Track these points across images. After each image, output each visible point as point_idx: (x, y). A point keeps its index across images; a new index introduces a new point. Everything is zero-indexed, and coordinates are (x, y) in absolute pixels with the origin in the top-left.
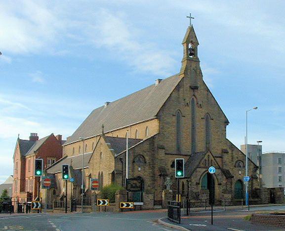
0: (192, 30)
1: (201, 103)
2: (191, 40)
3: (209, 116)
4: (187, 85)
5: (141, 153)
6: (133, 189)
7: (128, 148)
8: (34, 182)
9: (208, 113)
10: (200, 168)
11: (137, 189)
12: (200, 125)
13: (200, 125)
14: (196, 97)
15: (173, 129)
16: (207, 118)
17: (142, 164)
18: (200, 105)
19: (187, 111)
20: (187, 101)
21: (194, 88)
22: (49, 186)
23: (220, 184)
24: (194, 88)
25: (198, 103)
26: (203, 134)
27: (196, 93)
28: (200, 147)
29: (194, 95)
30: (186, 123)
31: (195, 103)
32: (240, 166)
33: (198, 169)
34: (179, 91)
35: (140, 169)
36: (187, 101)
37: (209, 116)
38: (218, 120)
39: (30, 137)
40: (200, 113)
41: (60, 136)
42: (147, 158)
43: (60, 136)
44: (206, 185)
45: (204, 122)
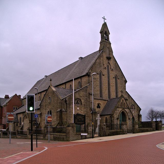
0: (105, 25)
1: (113, 68)
2: (105, 32)
3: (116, 76)
4: (105, 56)
5: (79, 98)
6: (79, 123)
7: (74, 91)
8: (161, 148)
9: (116, 75)
10: (118, 108)
11: (82, 123)
12: (113, 82)
13: (113, 82)
14: (110, 65)
15: (98, 82)
16: (116, 78)
17: (79, 105)
18: (112, 69)
19: (105, 72)
20: (105, 66)
21: (109, 58)
22: (12, 120)
23: (129, 119)
24: (109, 58)
25: (111, 68)
26: (114, 87)
27: (110, 62)
28: (113, 95)
29: (109, 63)
30: (105, 79)
31: (109, 68)
32: (133, 109)
33: (118, 109)
34: (100, 59)
35: (78, 108)
36: (105, 66)
37: (116, 76)
38: (121, 79)
39: (5, 97)
40: (112, 74)
41: (20, 96)
42: (83, 101)
43: (20, 96)
44: (122, 120)
45: (114, 80)
